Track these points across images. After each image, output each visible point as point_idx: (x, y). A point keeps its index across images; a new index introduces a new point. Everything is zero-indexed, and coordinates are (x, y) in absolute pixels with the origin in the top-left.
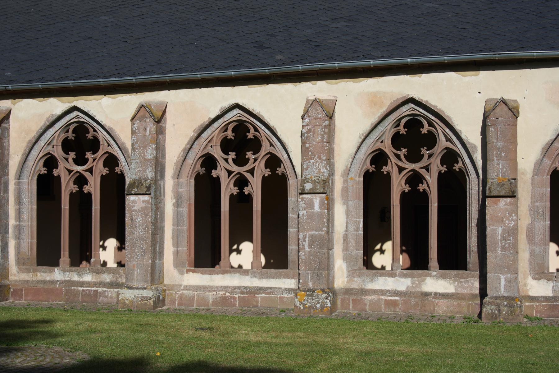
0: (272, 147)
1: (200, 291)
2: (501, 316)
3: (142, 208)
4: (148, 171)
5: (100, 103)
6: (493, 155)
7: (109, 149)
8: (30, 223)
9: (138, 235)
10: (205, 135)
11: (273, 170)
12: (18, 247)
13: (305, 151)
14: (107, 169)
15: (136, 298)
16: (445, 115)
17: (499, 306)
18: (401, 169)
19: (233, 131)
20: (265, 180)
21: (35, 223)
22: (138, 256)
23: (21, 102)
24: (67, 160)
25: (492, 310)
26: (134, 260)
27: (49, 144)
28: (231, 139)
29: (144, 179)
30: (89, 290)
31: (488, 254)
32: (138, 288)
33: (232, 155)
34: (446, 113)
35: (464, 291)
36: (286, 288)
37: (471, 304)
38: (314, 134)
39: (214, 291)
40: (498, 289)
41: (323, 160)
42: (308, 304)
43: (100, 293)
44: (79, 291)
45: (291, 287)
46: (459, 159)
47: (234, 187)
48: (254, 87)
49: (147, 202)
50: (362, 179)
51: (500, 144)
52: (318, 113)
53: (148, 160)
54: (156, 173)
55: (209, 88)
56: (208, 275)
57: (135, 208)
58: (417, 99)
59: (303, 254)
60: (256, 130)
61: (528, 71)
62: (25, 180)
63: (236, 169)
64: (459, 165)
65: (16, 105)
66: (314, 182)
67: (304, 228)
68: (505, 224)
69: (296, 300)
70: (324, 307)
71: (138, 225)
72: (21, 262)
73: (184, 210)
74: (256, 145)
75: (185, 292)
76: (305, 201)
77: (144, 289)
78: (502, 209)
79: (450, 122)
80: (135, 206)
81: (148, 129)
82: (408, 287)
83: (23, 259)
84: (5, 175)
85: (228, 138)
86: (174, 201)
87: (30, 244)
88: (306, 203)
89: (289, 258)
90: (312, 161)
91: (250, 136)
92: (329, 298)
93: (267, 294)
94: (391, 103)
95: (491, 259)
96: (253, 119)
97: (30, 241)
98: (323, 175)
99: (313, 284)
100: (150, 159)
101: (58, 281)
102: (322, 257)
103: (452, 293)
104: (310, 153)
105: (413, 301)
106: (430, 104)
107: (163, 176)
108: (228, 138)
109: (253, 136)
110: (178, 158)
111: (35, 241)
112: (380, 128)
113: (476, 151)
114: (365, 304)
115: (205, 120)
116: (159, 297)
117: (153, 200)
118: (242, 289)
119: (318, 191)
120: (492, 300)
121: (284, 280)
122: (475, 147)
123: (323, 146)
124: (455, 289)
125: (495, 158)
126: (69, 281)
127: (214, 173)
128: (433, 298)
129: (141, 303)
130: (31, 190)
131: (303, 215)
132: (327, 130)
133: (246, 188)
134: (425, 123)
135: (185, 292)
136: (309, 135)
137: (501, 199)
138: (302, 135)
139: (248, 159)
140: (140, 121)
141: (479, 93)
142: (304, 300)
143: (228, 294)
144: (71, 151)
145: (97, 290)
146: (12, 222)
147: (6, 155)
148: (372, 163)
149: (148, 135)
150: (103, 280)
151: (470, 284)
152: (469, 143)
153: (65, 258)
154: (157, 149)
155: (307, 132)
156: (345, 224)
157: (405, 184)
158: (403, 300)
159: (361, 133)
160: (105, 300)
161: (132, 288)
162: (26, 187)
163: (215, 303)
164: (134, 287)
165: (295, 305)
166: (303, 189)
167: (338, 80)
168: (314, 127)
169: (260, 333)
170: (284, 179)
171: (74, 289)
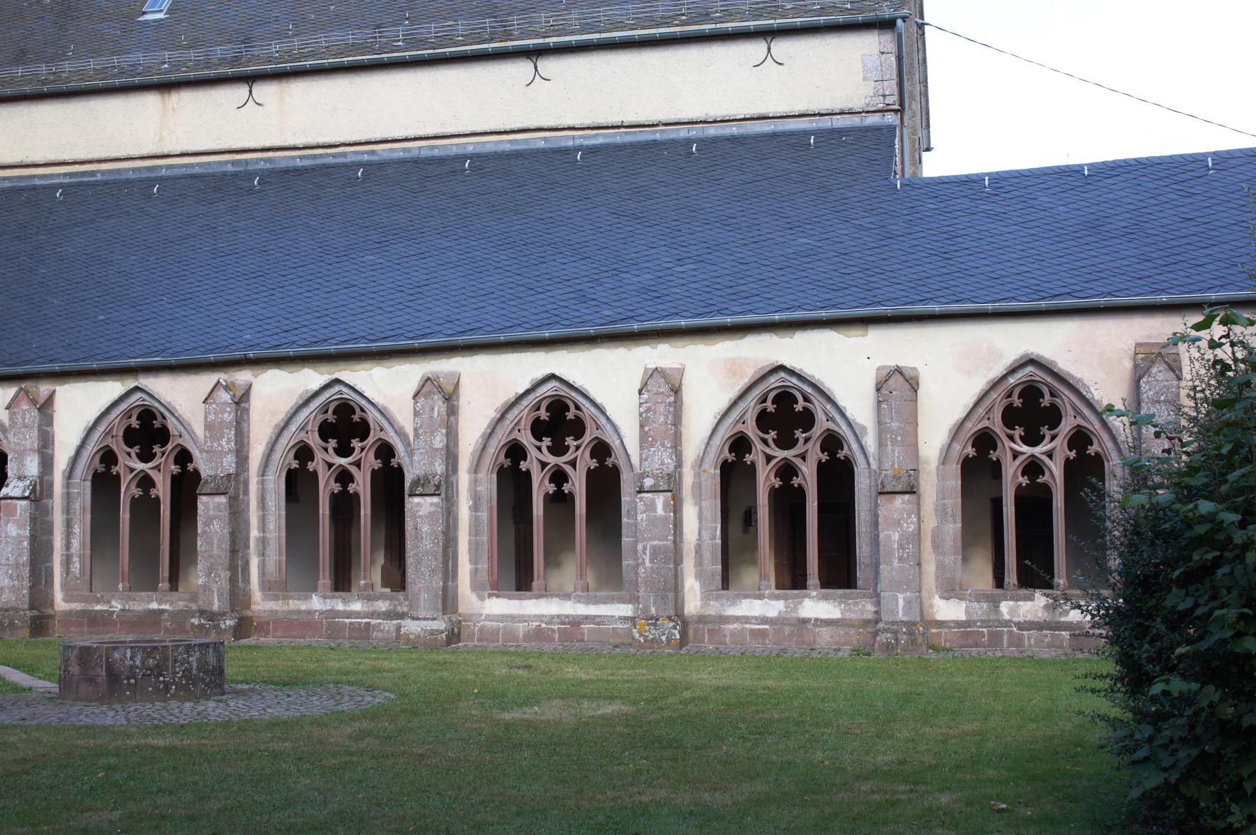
1: (507, 621)
3: (429, 513)
4: (437, 464)
5: (370, 375)
6: (887, 439)
7: (382, 435)
10: (511, 416)
12: (262, 566)
13: (644, 437)
14: (379, 461)
17: (895, 633)
19: (547, 410)
20: (821, 466)
24: (326, 450)
25: (887, 639)
27: (302, 429)
31: (881, 567)
32: (425, 619)
33: (333, 443)
35: (853, 616)
39: (525, 621)
40: (894, 611)
41: (667, 448)
43: (374, 626)
44: (345, 624)
45: (627, 615)
47: (336, 482)
49: (436, 505)
50: (718, 471)
53: (437, 450)
54: (447, 467)
57: (420, 513)
59: (643, 570)
60: (578, 408)
63: (552, 460)
66: (656, 477)
69: (634, 630)
72: (266, 586)
73: (484, 515)
74: (807, 420)
75: (487, 623)
77: (434, 619)
81: (436, 409)
82: (780, 612)
83: (270, 582)
84: (245, 471)
86: (471, 502)
88: (645, 505)
90: (652, 449)
92: (678, 628)
94: (755, 372)
96: (573, 394)
99: (656, 610)
101: (316, 611)
104: (650, 439)
105: (787, 630)
106: (805, 373)
107: (455, 471)
115: (511, 396)
116: (453, 630)
117: (444, 502)
118: (563, 619)
119: (661, 488)
121: (618, 606)
124: (842, 614)
125: (889, 443)
126: (331, 611)
131: (642, 520)
132: (672, 409)
133: (565, 484)
135: (487, 623)
137: (897, 496)
138: (641, 415)
139: (568, 447)
142: (646, 631)
143: (543, 625)
146: (254, 533)
150: (377, 609)
151: (860, 606)
154: (448, 435)
155: (646, 412)
156: (697, 531)
159: (717, 411)
160: (380, 635)
161: (418, 619)
162: (272, 486)
163: (528, 637)
165: (633, 638)
166: (642, 486)
170: (615, 471)
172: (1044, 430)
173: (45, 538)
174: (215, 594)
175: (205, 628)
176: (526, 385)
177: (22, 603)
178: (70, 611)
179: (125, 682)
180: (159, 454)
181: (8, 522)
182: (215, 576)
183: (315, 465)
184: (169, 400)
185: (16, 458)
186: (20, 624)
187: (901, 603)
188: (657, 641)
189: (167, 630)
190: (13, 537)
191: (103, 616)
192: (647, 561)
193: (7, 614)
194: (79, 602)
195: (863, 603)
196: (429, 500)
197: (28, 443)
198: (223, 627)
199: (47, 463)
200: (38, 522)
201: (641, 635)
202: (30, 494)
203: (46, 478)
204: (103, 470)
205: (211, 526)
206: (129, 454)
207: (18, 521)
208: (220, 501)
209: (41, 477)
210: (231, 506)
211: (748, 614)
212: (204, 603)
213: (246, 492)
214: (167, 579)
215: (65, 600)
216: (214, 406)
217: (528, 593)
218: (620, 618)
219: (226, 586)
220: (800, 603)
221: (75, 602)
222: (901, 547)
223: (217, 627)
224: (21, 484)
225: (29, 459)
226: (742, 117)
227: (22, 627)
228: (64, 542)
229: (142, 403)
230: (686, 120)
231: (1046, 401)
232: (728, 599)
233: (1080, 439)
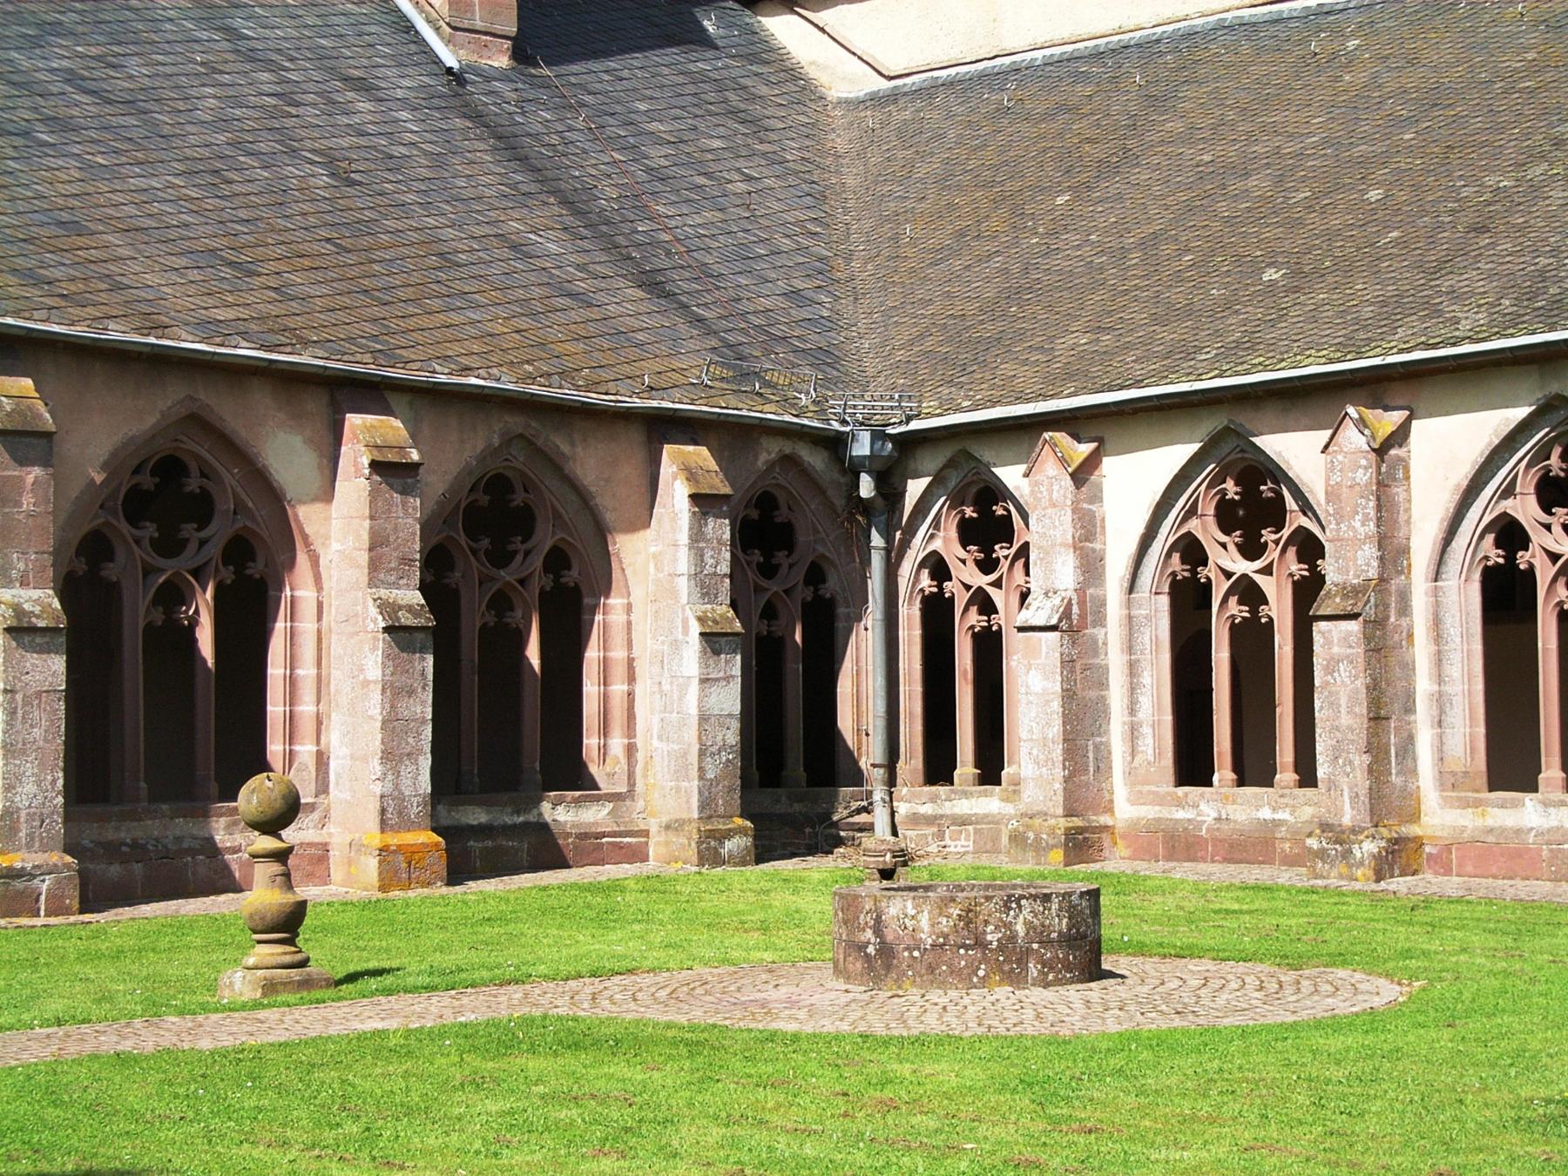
8: (1466, 687)
11: (500, 615)
21: (1479, 686)
28: (1557, 477)
62: (1450, 583)
83: (1453, 774)
84: (1400, 573)
87: (1467, 738)
97: (1468, 730)
101: (1532, 829)
111: (1481, 730)
130: (1466, 606)
144: (1559, 506)
146: (1423, 685)
147: (1402, 523)
153: (1223, 773)
169: (1483, 960)
173: (1093, 694)
174: (1346, 794)
177: (1054, 806)
180: (1271, 545)
183: (1209, 572)
185: (1042, 559)
194: (1153, 803)
199: (1091, 567)
200: (1078, 666)
202: (1060, 620)
203: (1090, 591)
204: (1186, 574)
206: (1224, 546)
209: (1081, 591)
210: (1368, 638)
213: (1405, 609)
214: (1291, 768)
216: (1340, 457)
219: (1363, 783)
224: (1048, 604)
225: (1060, 561)
228: (1126, 701)
229: (1240, 455)
231: (193, 484)
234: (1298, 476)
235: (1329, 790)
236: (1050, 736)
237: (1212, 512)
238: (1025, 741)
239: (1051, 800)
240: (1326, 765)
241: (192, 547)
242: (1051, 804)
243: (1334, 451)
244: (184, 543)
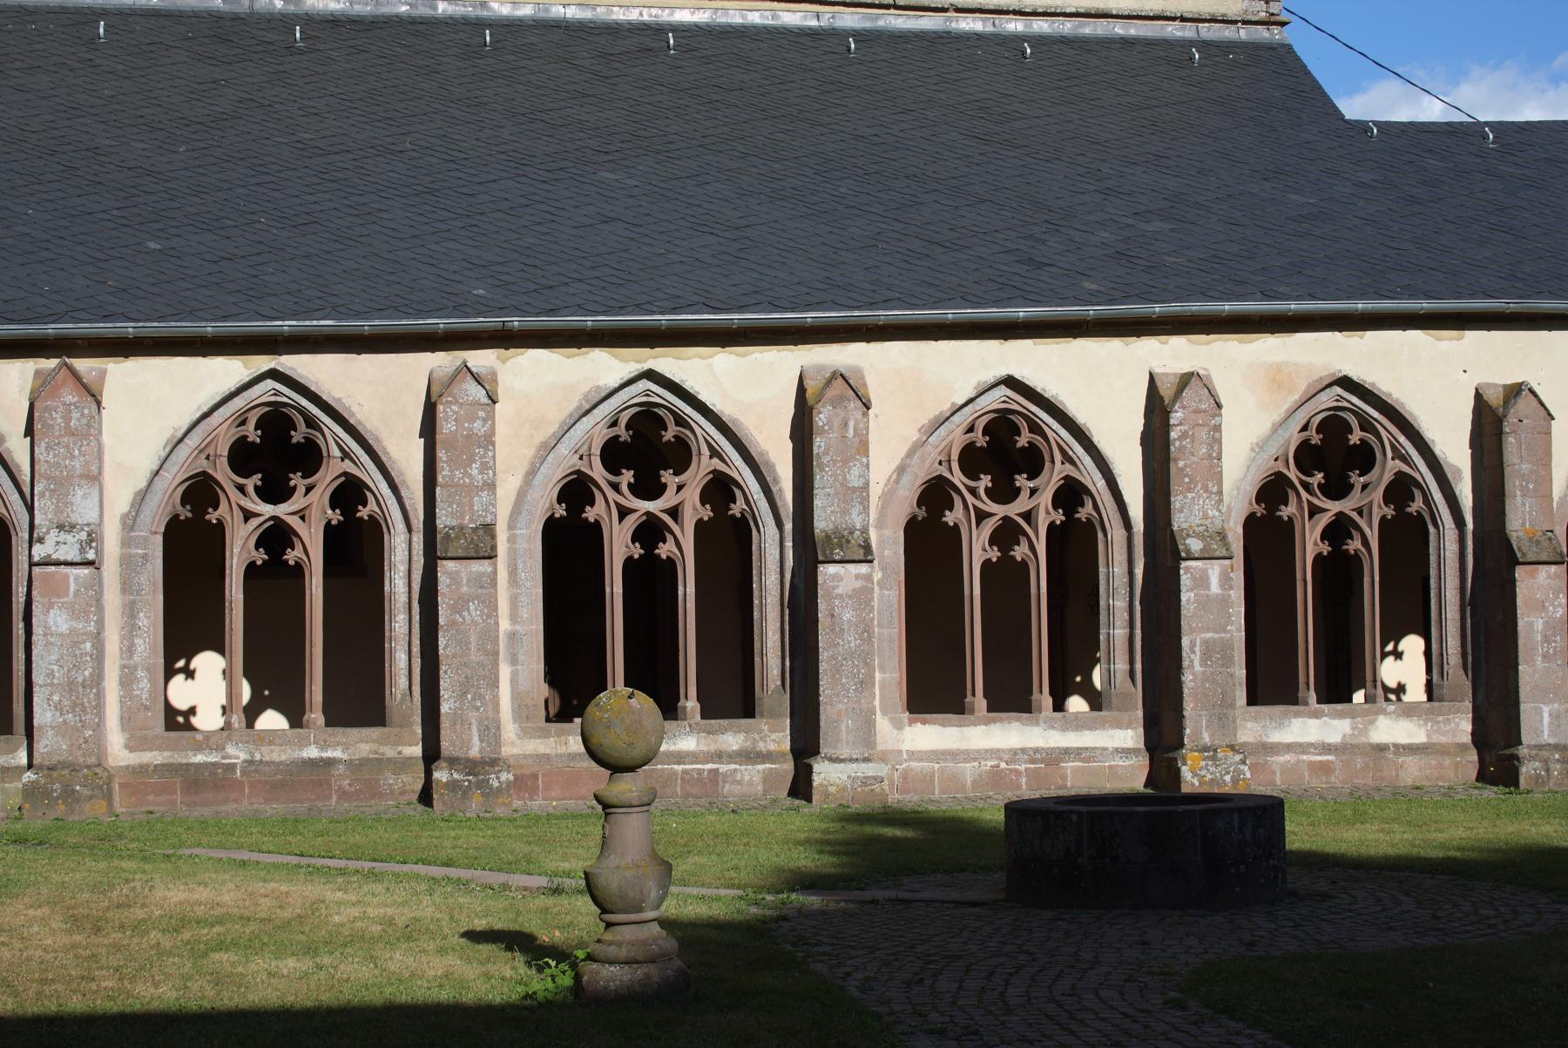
0: (347, 461)
1: (945, 760)
2: (1552, 781)
3: (853, 590)
5: (710, 366)
6: (1515, 487)
9: (846, 647)
15: (850, 781)
16: (1406, 411)
17: (1546, 761)
18: (248, 515)
20: (330, 530)
22: (848, 691)
23: (520, 357)
25: (1535, 770)
26: (840, 702)
27: (201, 451)
29: (846, 529)
30: (698, 769)
31: (1520, 667)
32: (851, 760)
34: (1408, 408)
35: (1443, 739)
36: (1117, 749)
37: (1460, 762)
38: (1193, 442)
39: (975, 760)
40: (1538, 731)
41: (1212, 493)
42: (1209, 776)
43: (725, 775)
44: (674, 773)
45: (1125, 746)
46: (738, 493)
48: (1046, 344)
51: (1525, 467)
52: (1200, 401)
55: (953, 342)
56: (955, 728)
57: (839, 591)
58: (1355, 378)
59: (1191, 677)
61: (1545, 333)
64: (368, 508)
65: (509, 364)
67: (1190, 627)
68: (1548, 612)
70: (1238, 781)
71: (846, 627)
74: (310, 458)
75: (914, 764)
76: (1192, 573)
78: (1542, 586)
79: (1415, 425)
80: (838, 586)
81: (851, 424)
82: (1345, 736)
85: (621, 439)
88: (1193, 578)
89: (15, 712)
90: (1190, 495)
91: (297, 437)
93: (1083, 761)
94: (1309, 385)
95: (1527, 677)
96: (304, 402)
98: (1212, 523)
99: (1212, 736)
100: (858, 488)
102: (1228, 682)
103: (1424, 744)
104: (1187, 480)
105: (1359, 762)
106: (1379, 389)
108: (621, 439)
109: (1028, 442)
110: (886, 485)
112: (587, 422)
113: (1461, 478)
114: (1274, 773)
115: (946, 407)
118: (1033, 754)
120: (1534, 752)
122: (1458, 471)
123: (1211, 466)
124: (1428, 736)
125: (1518, 493)
127: (591, 514)
128: (1395, 753)
129: (863, 791)
131: (1188, 601)
134: (300, 421)
135: (914, 764)
136: (1184, 443)
137: (1541, 567)
140: (834, 407)
141: (1465, 371)
142: (1201, 769)
143: (1003, 765)
145: (717, 770)
148: (184, 502)
149: (851, 436)
150: (724, 747)
151: (1453, 725)
152: (1448, 463)
157: (257, 548)
158: (1342, 761)
159: (1255, 441)
160: (737, 789)
164: (842, 757)
167: (1212, 337)
168: (1193, 428)
171: (663, 770)
172: (296, 480)
175: (460, 787)
176: (970, 392)
178: (141, 766)
179: (1233, 870)
181: (51, 606)
182: (474, 699)
184: (337, 396)
186: (87, 792)
187: (1546, 716)
188: (1218, 784)
189: (343, 795)
190: (61, 635)
191: (213, 774)
192: (1197, 663)
193: (55, 774)
194: (160, 749)
195: (1457, 720)
196: (853, 569)
197: (77, 464)
198: (496, 784)
201: (1195, 775)
205: (465, 614)
207: (72, 605)
208: (482, 569)
211: (1301, 740)
212: (453, 744)
215: (130, 747)
216: (455, 408)
217: (971, 718)
218: (1117, 750)
220: (1372, 722)
221: (151, 750)
222: (1546, 639)
223: (483, 784)
225: (80, 493)
226: (1073, 10)
227: (91, 798)
230: (992, 7)
232: (1271, 719)
233: (720, 489)
234: (360, 423)
235: (455, 724)
236: (80, 680)
237: (226, 454)
238: (41, 686)
239: (79, 748)
240: (452, 700)
241: (1025, 494)
242: (79, 753)
243: (447, 402)
244: (1018, 491)
